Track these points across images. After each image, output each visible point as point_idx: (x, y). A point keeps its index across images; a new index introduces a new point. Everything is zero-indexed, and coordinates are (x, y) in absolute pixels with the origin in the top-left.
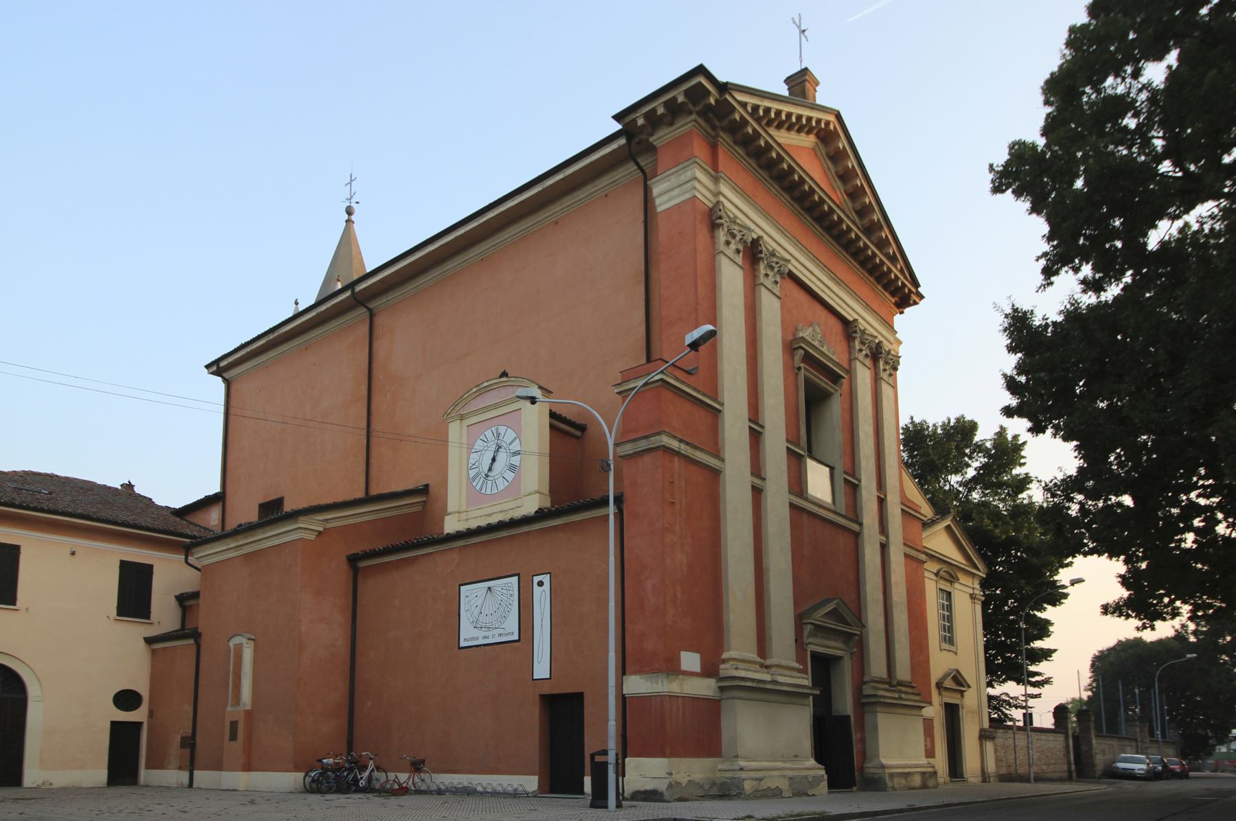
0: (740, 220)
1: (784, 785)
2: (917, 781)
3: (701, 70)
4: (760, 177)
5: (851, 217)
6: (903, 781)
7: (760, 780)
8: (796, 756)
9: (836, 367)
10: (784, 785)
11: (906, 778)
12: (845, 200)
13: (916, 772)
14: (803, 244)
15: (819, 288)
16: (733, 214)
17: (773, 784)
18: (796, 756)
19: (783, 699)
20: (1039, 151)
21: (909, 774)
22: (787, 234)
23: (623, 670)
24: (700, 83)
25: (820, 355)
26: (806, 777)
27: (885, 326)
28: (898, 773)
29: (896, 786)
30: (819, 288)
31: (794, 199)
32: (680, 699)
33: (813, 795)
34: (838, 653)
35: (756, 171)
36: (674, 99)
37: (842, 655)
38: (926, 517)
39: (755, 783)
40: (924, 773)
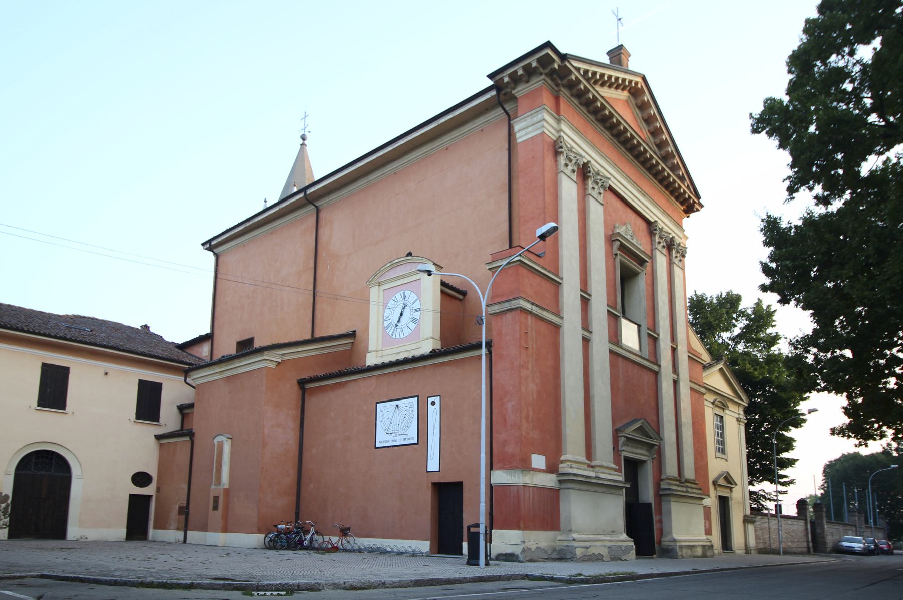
1: (604, 552)
2: (699, 551)
3: (548, 45)
5: (653, 149)
7: (587, 548)
8: (613, 532)
10: (604, 552)
11: (691, 550)
18: (613, 532)
21: (694, 546)
24: (548, 54)
25: (631, 245)
30: (630, 198)
38: (705, 362)
39: (584, 550)
40: (704, 546)
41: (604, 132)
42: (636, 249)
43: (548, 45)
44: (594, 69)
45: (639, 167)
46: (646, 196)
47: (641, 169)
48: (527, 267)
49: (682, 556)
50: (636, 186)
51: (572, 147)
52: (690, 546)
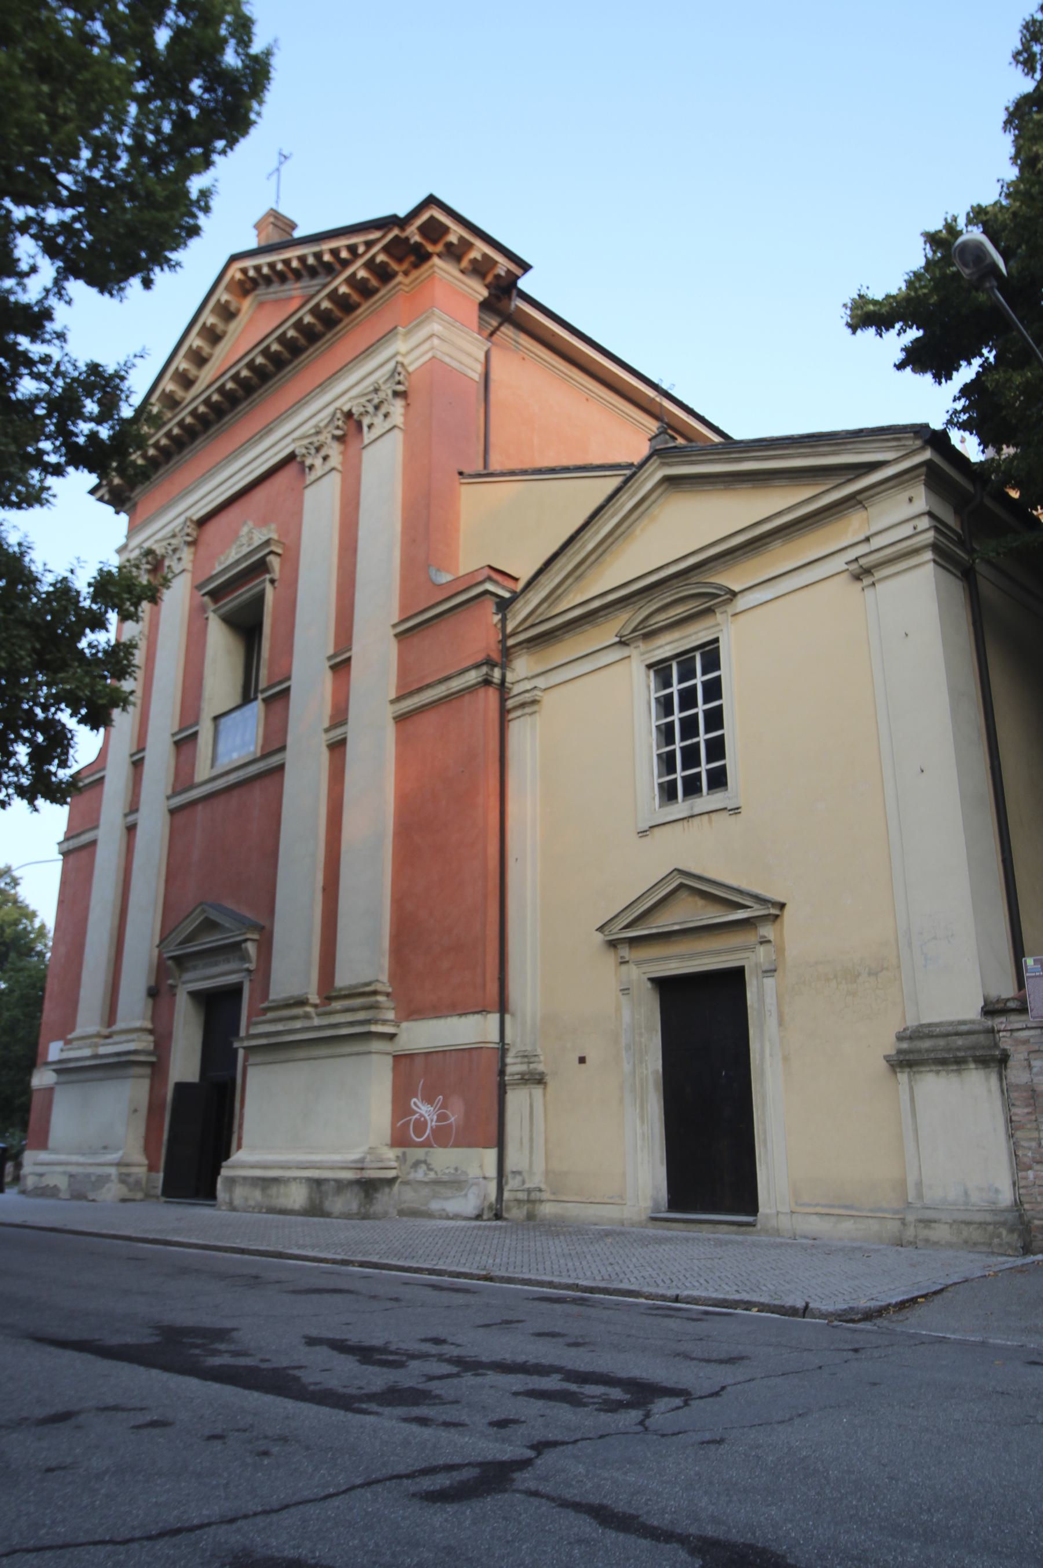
0: (322, 420)
1: (62, 1183)
2: (297, 1197)
3: (431, 201)
4: (381, 302)
5: (317, 288)
6: (257, 1195)
7: (41, 1175)
8: (105, 1148)
9: (250, 558)
10: (62, 1183)
11: (264, 1190)
12: (301, 288)
13: (295, 1179)
14: (309, 390)
15: (276, 454)
16: (311, 428)
17: (50, 1181)
18: (105, 1148)
19: (100, 1074)
20: (127, 11)
21: (276, 1180)
22: (192, 487)
23: (244, 1048)
24: (432, 218)
25: (225, 574)
26: (88, 1175)
27: (290, 415)
28: (245, 1178)
29: (238, 1202)
30: (276, 454)
31: (246, 398)
32: (419, 1062)
33: (93, 1200)
34: (233, 979)
35: (236, 415)
36: (470, 246)
37: (240, 980)
38: (516, 579)
39: (36, 1178)
40: (318, 1182)
41: (239, 413)
42: (236, 567)
43: (431, 201)
44: (316, 249)
45: (266, 391)
46: (272, 426)
47: (308, 357)
48: (883, 487)
49: (231, 1203)
50: (307, 398)
51: (316, 426)
52: (264, 1180)
